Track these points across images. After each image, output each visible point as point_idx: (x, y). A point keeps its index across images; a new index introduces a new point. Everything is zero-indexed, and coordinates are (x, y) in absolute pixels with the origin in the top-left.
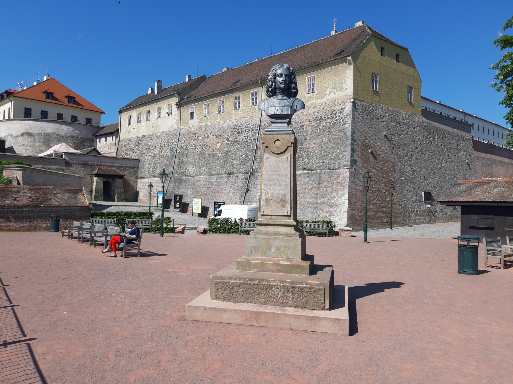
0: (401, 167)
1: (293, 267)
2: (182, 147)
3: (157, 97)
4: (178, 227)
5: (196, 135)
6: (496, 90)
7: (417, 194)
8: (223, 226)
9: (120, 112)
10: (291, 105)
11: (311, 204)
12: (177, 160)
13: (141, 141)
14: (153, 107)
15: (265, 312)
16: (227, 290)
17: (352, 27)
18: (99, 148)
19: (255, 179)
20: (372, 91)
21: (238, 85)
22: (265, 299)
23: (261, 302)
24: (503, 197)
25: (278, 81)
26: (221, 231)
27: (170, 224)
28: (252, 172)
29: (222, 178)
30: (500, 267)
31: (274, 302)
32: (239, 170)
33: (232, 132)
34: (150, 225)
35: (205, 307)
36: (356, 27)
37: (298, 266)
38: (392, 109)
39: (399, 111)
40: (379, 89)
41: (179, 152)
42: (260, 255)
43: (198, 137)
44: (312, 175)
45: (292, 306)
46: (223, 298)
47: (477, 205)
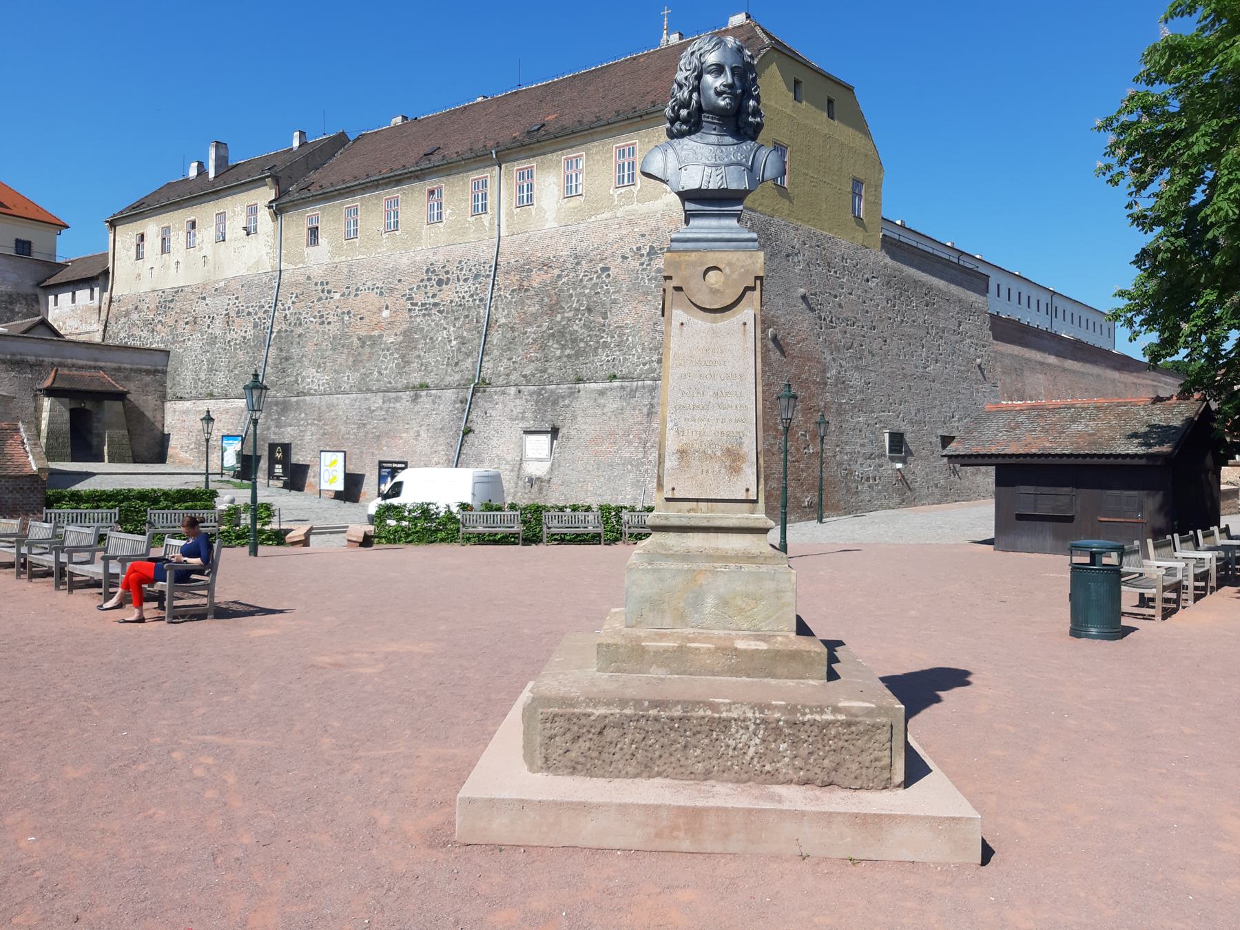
0: (839, 373)
1: (778, 658)
2: (285, 317)
3: (216, 185)
4: (291, 530)
5: (326, 288)
6: (1107, 182)
7: (872, 437)
8: (416, 525)
9: (113, 224)
10: (750, 163)
11: (632, 465)
12: (273, 351)
13: (172, 301)
14: (205, 213)
15: (718, 809)
16: (581, 740)
17: (723, 26)
18: (55, 320)
19: (486, 401)
20: (774, 186)
21: (436, 159)
22: (706, 763)
23: (692, 773)
24: (1095, 443)
25: (710, 88)
26: (410, 538)
27: (270, 522)
28: (478, 383)
29: (397, 399)
30: (1154, 616)
31: (733, 773)
32: (442, 380)
33: (422, 281)
34: (216, 524)
35: (522, 801)
36: (730, 26)
37: (794, 655)
38: (819, 231)
39: (833, 238)
40: (790, 183)
41: (278, 332)
42: (668, 620)
43: (329, 292)
44: (632, 393)
45: (790, 782)
46: (569, 764)
47: (1120, 463)
